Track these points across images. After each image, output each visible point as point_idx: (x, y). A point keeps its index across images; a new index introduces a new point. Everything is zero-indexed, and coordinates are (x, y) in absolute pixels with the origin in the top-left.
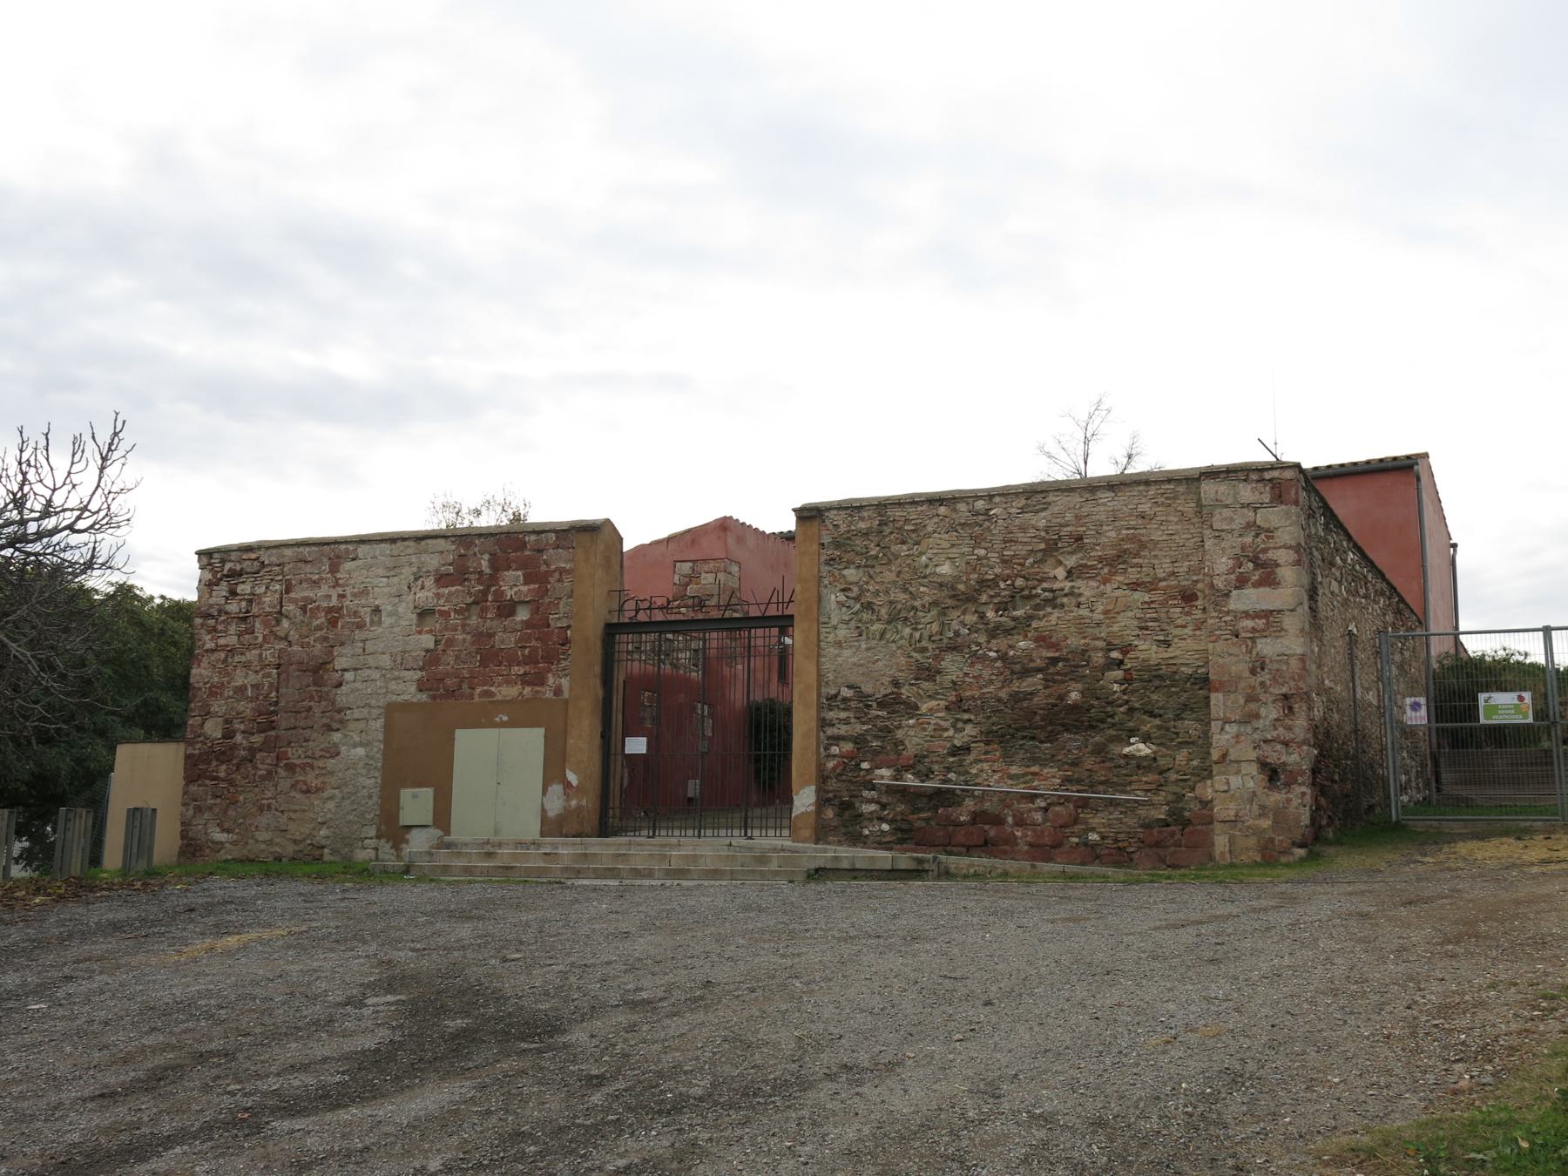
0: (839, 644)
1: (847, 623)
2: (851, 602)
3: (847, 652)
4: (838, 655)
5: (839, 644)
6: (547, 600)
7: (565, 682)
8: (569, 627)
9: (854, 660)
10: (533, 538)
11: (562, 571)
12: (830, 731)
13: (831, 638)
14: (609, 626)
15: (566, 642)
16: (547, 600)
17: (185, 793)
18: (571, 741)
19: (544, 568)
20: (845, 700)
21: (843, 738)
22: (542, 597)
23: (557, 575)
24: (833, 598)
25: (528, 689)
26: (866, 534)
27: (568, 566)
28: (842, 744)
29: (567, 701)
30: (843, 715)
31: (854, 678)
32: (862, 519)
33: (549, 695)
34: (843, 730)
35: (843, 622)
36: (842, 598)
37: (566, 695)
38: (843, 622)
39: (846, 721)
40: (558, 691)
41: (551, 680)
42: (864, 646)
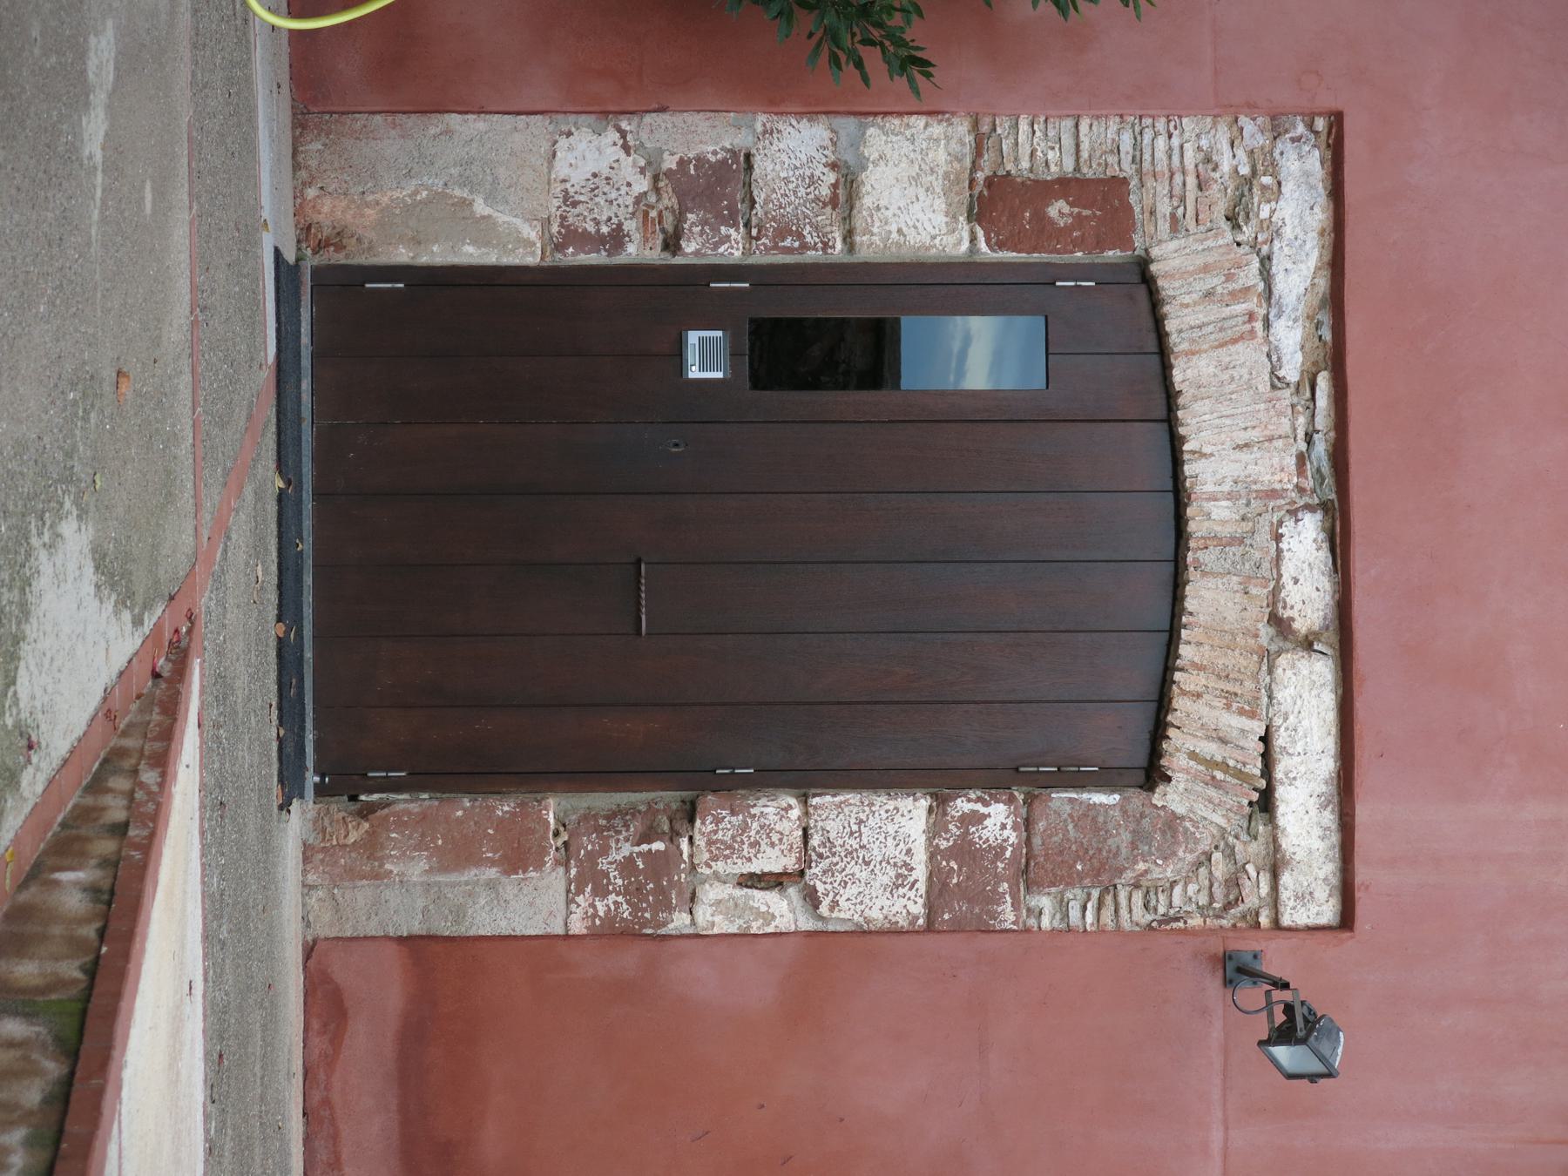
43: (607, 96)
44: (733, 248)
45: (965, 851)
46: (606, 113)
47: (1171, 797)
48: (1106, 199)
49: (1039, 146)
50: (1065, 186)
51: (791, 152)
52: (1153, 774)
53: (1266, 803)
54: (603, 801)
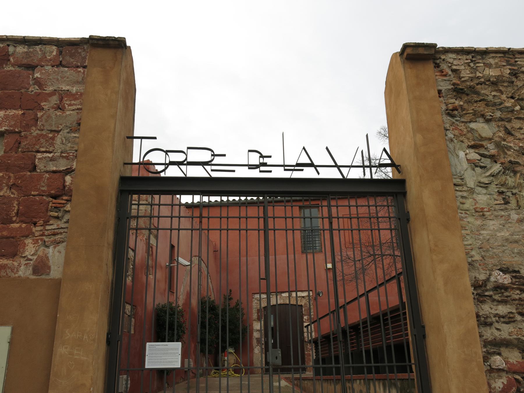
0: (480, 213)
1: (486, 186)
2: (487, 162)
3: (493, 224)
4: (482, 227)
5: (480, 213)
6: (35, 132)
7: (56, 256)
8: (69, 171)
9: (505, 234)
10: (21, 49)
11: (63, 95)
12: (489, 333)
13: (468, 204)
14: (124, 180)
15: (62, 193)
16: (35, 132)
17: (71, 196)
18: (61, 351)
19: (34, 89)
20: (499, 288)
21: (506, 344)
22: (27, 127)
23: (54, 100)
24: (463, 156)
25: (24, 225)
26: (494, 83)
27: (74, 90)
28: (504, 351)
29: (57, 284)
30: (502, 310)
31: (508, 259)
32: (489, 66)
33: (25, 272)
34: (505, 331)
35: (481, 184)
36: (473, 155)
37: (56, 272)
38: (481, 184)
39: (509, 319)
40: (41, 267)
41: (30, 248)
42: (514, 216)
43: (252, 350)
44: (263, 339)
45: (308, 320)
46: (253, 349)
47: (303, 304)
48: (259, 311)
49: (255, 316)
50: (258, 314)
51: (256, 335)
52: (301, 306)
53: (303, 297)
54: (305, 348)
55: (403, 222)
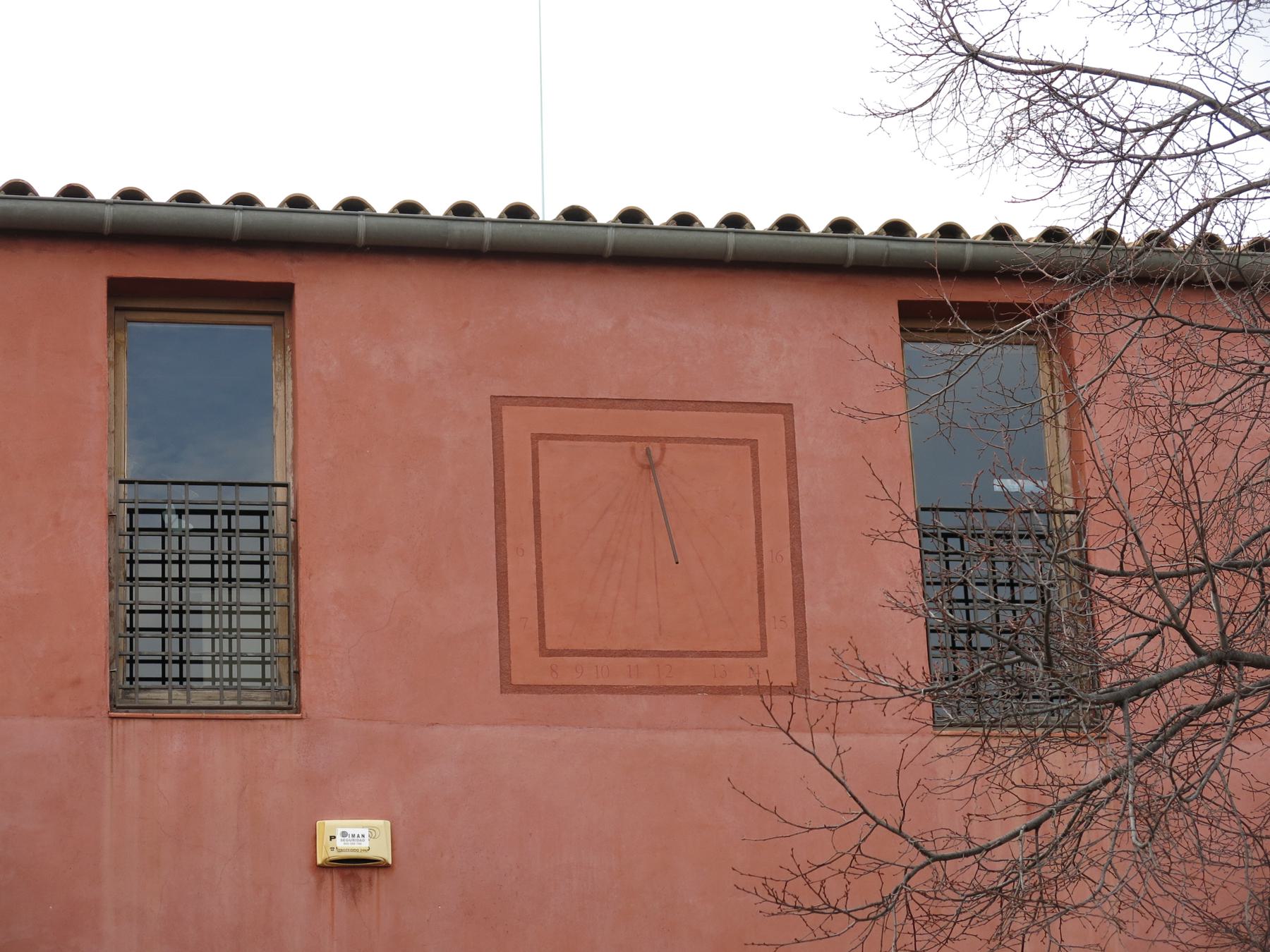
55: (505, 672)
